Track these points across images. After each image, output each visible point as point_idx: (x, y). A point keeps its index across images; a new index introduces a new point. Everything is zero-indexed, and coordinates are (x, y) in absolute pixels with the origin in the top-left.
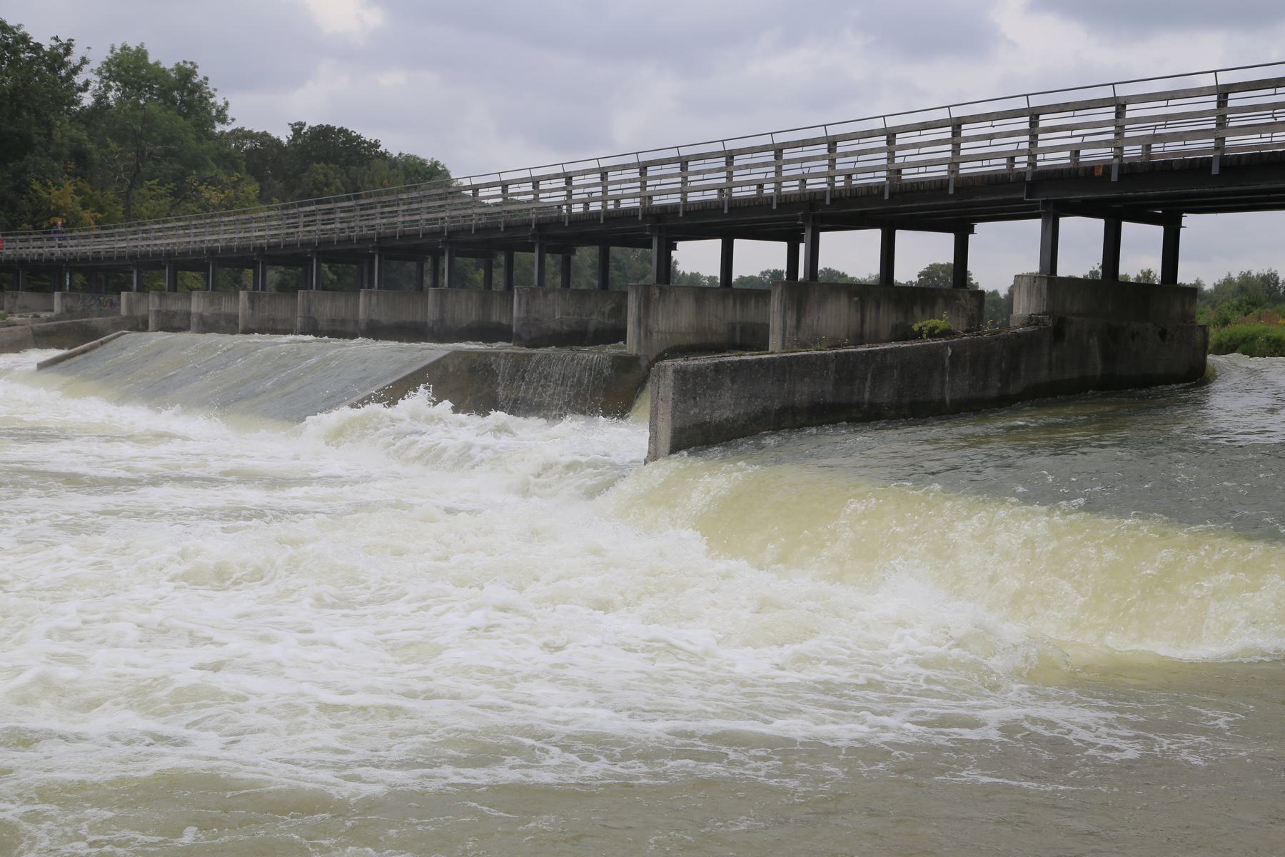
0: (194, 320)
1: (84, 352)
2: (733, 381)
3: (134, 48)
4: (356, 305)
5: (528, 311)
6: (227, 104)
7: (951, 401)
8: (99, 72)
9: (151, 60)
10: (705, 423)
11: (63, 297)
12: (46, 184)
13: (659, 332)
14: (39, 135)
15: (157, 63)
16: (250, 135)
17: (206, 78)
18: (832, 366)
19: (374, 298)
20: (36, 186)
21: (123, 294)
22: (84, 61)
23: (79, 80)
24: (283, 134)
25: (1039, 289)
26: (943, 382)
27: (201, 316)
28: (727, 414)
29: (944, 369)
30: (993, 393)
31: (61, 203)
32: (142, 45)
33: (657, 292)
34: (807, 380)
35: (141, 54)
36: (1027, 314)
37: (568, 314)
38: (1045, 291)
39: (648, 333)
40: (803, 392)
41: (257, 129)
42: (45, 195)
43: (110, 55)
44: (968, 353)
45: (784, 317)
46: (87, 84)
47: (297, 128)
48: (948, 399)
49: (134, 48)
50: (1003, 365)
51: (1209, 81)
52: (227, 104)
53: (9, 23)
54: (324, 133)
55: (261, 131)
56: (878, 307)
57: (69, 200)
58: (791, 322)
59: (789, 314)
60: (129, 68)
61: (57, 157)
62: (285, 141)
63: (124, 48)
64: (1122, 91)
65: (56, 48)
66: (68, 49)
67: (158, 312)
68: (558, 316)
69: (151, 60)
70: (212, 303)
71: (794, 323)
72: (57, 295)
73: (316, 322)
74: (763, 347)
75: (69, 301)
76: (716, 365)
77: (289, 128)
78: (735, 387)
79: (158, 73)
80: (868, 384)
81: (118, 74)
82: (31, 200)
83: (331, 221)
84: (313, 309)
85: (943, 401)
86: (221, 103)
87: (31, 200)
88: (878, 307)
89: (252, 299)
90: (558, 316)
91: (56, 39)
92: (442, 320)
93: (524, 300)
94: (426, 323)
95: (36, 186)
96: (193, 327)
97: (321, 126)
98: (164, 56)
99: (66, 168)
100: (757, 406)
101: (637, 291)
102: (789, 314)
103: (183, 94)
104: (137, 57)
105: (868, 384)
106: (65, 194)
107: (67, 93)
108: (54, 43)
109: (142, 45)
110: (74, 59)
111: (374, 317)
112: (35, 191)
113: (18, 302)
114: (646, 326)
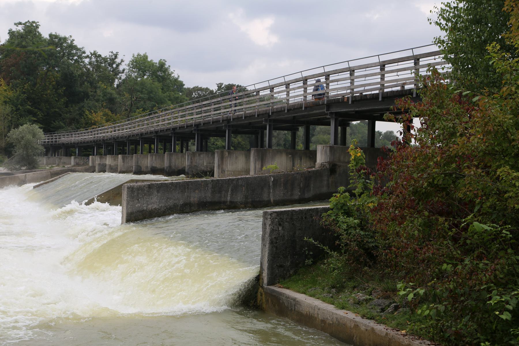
0: (107, 167)
1: (52, 181)
2: (158, 192)
3: (142, 55)
4: (163, 161)
5: (191, 162)
6: (179, 76)
7: (274, 201)
8: (129, 66)
9: (149, 60)
10: (144, 210)
11: (75, 158)
12: (91, 112)
13: (228, 171)
14: (92, 92)
15: (151, 61)
16: (201, 89)
17: (169, 66)
18: (210, 186)
19: (154, 157)
20: (87, 113)
21: (90, 157)
22: (122, 61)
23: (121, 68)
24: (214, 88)
25: (326, 152)
26: (269, 193)
27: (110, 165)
28: (155, 206)
29: (269, 186)
30: (296, 197)
31: (96, 119)
32: (146, 53)
33: (227, 153)
34: (197, 191)
35: (145, 57)
36: (320, 162)
37: (210, 163)
38: (328, 152)
39: (223, 171)
40: (195, 197)
41: (204, 86)
42: (90, 117)
43: (133, 58)
44: (282, 180)
45: (255, 164)
46: (124, 70)
47: (220, 86)
48: (272, 200)
49: (142, 55)
50: (302, 185)
51: (375, 60)
52: (179, 76)
53: (79, 47)
54: (230, 87)
55: (205, 87)
56: (301, 159)
57: (99, 118)
58: (258, 166)
59: (257, 163)
60: (141, 64)
61: (97, 101)
62: (215, 91)
63: (138, 55)
64: (352, 64)
65: (112, 56)
66: (116, 57)
67: (99, 164)
68: (205, 164)
69: (149, 60)
70: (115, 160)
71: (260, 166)
72: (73, 157)
73: (141, 167)
74: (213, 175)
75: (77, 160)
76: (149, 185)
77: (216, 85)
78: (159, 194)
79: (152, 64)
80: (229, 193)
81: (136, 66)
82: (85, 118)
83: (143, 125)
84: (139, 162)
85: (269, 201)
86: (176, 76)
87: (85, 118)
88: (301, 159)
89: (123, 159)
90: (205, 164)
91: (112, 52)
92: (170, 167)
93: (190, 157)
94: (164, 168)
95: (87, 113)
96: (107, 170)
97: (229, 84)
98: (154, 58)
99: (102, 105)
100: (171, 203)
101: (218, 153)
102: (257, 163)
103: (159, 73)
104: (144, 59)
105: (229, 193)
106: (98, 116)
107: (116, 72)
108: (111, 54)
109: (146, 53)
110: (118, 61)
111: (154, 165)
112: (87, 115)
113: (62, 161)
114: (222, 168)
